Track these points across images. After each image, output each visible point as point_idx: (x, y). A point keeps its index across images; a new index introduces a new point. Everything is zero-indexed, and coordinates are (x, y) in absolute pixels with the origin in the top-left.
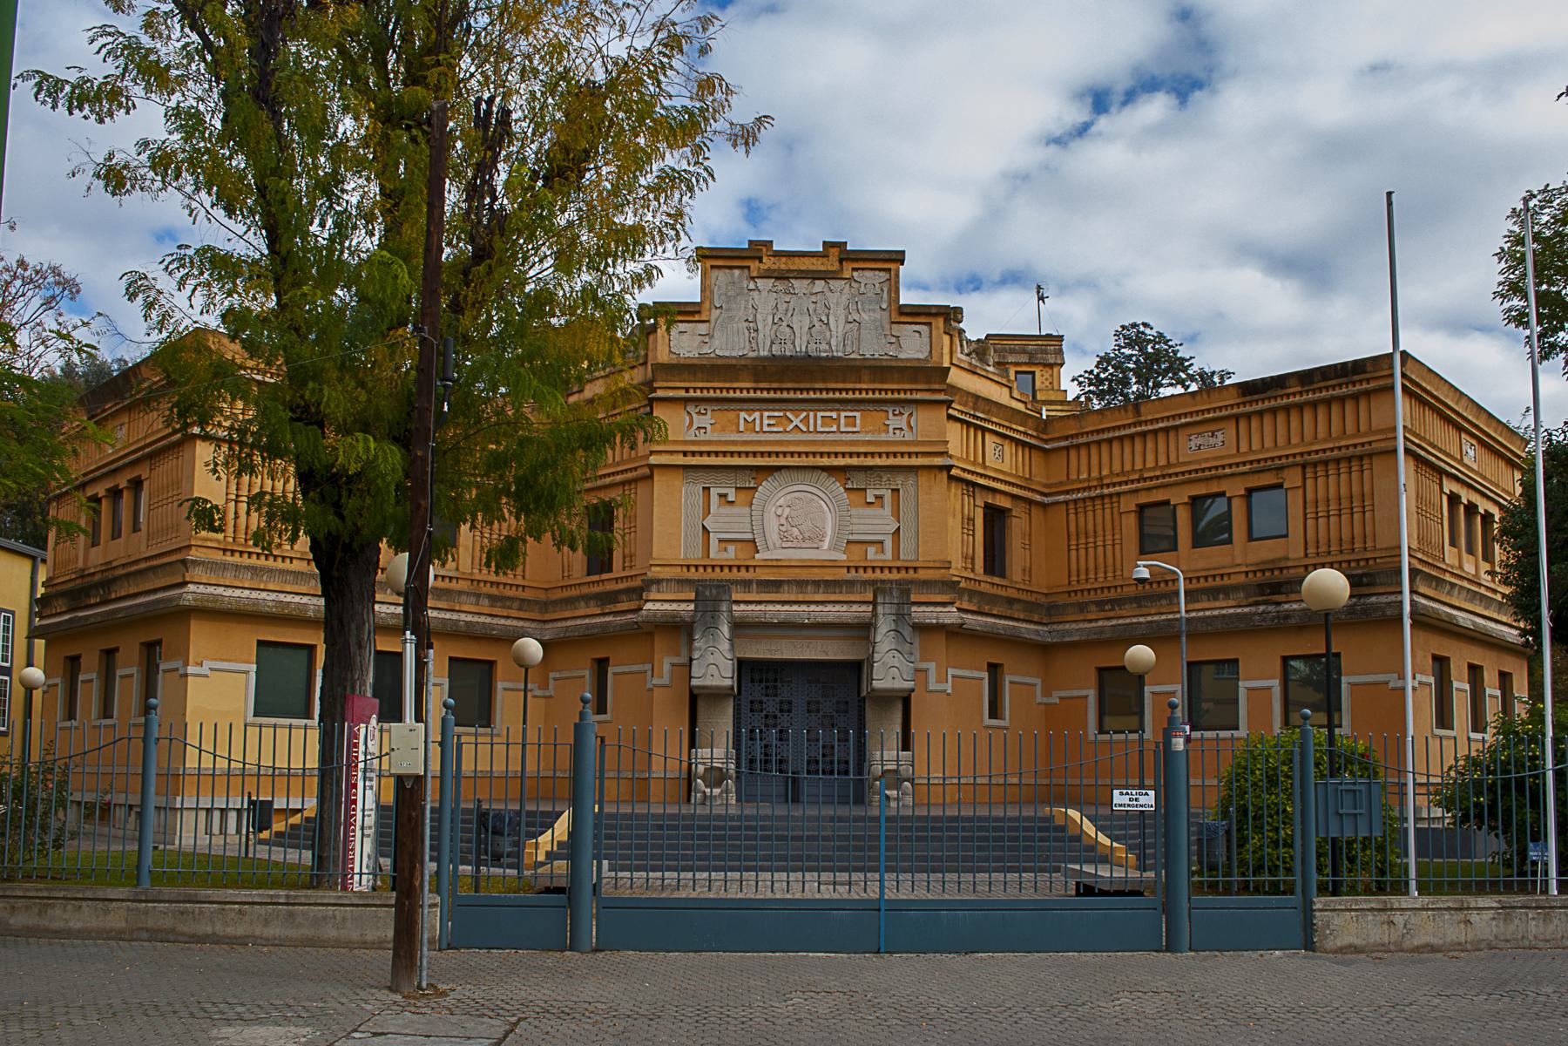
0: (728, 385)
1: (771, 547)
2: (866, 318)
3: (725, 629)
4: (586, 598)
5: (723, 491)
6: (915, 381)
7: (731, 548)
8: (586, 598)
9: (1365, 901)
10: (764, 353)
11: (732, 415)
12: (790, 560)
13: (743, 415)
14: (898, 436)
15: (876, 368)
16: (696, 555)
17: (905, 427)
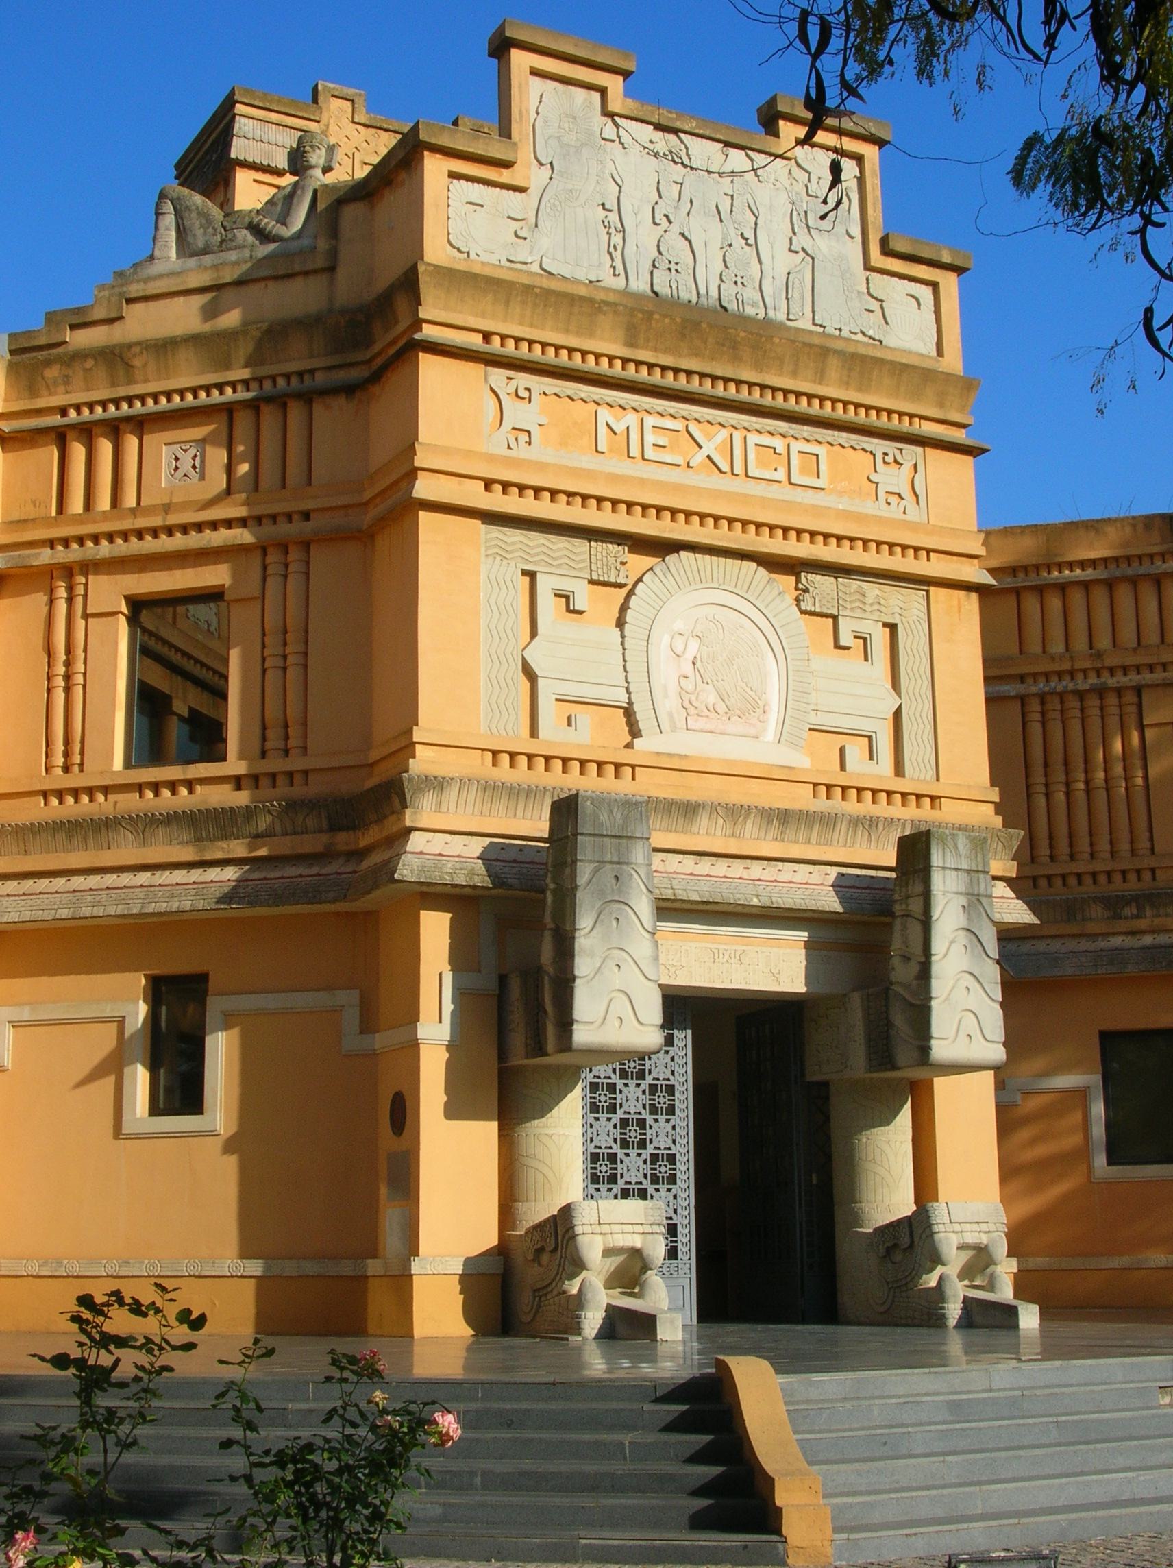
0: (573, 342)
1: (665, 726)
2: (824, 249)
3: (644, 907)
4: (145, 824)
5: (565, 585)
6: (916, 396)
7: (585, 717)
8: (145, 824)
9: (438, 1494)
10: (640, 285)
11: (582, 412)
12: (681, 757)
13: (605, 415)
14: (894, 512)
15: (855, 357)
16: (517, 737)
17: (907, 493)
